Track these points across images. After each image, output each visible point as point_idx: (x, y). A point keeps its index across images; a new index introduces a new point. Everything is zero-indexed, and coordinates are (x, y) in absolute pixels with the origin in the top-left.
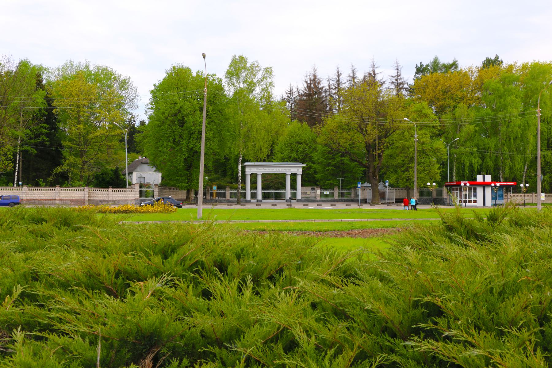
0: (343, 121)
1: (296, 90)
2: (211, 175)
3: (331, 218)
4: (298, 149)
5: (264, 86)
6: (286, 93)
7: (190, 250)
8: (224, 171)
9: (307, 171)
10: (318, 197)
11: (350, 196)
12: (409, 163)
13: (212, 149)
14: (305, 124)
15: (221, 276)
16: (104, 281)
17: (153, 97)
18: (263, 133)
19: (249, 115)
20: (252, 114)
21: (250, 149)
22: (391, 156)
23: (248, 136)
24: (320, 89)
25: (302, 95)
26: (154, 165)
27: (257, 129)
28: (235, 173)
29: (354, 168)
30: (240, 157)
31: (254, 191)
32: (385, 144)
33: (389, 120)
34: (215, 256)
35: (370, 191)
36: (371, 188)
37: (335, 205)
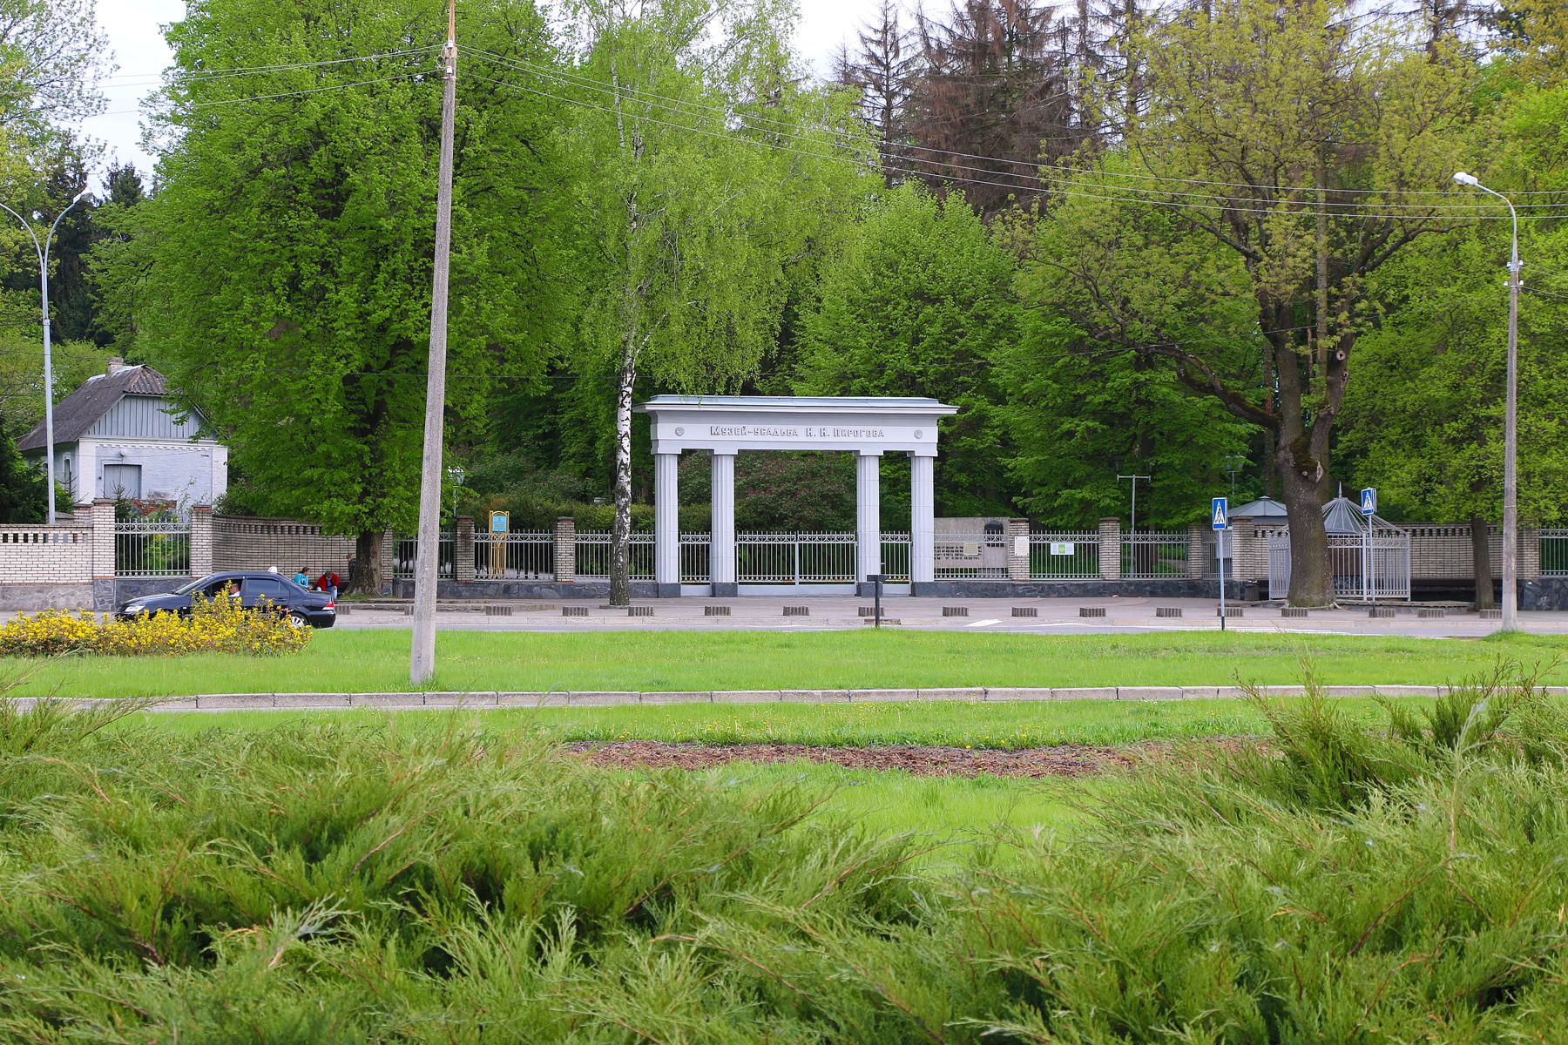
0: (1148, 187)
1: (913, 24)
2: (479, 454)
3: (1066, 683)
4: (920, 329)
5: (750, 13)
6: (864, 40)
7: (389, 832)
8: (545, 436)
9: (967, 441)
10: (1021, 573)
11: (1180, 564)
12: (1483, 401)
13: (484, 329)
14: (955, 202)
15: (481, 909)
16: (133, 928)
17: (183, 59)
18: (744, 248)
19: (671, 159)
20: (686, 155)
21: (676, 329)
22: (1391, 364)
23: (667, 267)
24: (1035, 19)
25: (942, 52)
26: (191, 409)
27: (711, 229)
28: (600, 449)
29: (1201, 424)
30: (624, 371)
31: (697, 540)
32: (1363, 305)
33: (1381, 180)
34: (466, 853)
35: (1285, 542)
36: (1285, 529)
37: (1100, 613)
